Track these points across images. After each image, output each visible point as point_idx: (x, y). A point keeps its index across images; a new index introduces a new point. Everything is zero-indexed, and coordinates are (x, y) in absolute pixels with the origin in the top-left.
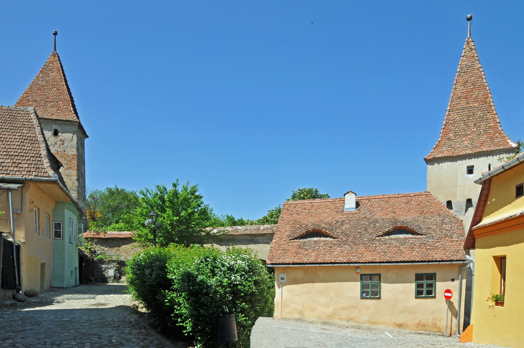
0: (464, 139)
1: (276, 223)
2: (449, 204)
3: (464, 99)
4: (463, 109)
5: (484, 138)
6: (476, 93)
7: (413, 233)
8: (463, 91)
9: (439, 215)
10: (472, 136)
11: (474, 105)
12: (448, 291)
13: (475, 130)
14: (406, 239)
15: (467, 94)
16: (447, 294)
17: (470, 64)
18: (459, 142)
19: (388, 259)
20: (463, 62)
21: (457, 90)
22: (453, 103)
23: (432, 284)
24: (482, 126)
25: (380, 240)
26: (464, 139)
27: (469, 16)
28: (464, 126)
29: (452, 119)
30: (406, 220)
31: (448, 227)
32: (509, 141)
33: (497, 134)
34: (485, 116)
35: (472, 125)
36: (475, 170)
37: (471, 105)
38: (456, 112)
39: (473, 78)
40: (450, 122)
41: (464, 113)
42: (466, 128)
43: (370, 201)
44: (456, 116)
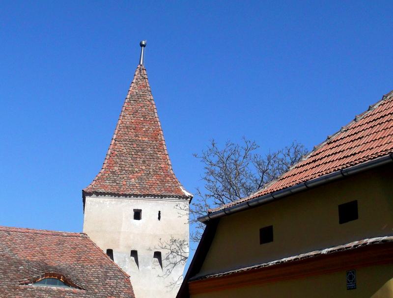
0: (131, 176)
1: (355, 288)
2: (110, 252)
3: (133, 131)
4: (132, 142)
5: (153, 179)
6: (147, 127)
7: (67, 283)
8: (133, 121)
9: (101, 266)
10: (140, 174)
14: (60, 292)
17: (141, 93)
20: (134, 89)
21: (126, 118)
25: (25, 289)
26: (131, 176)
28: (132, 161)
29: (118, 150)
30: (60, 266)
31: (113, 282)
32: (181, 188)
36: (143, 215)
37: (140, 139)
38: (124, 143)
39: (144, 110)
40: (116, 153)
43: (9, 234)
44: (122, 148)
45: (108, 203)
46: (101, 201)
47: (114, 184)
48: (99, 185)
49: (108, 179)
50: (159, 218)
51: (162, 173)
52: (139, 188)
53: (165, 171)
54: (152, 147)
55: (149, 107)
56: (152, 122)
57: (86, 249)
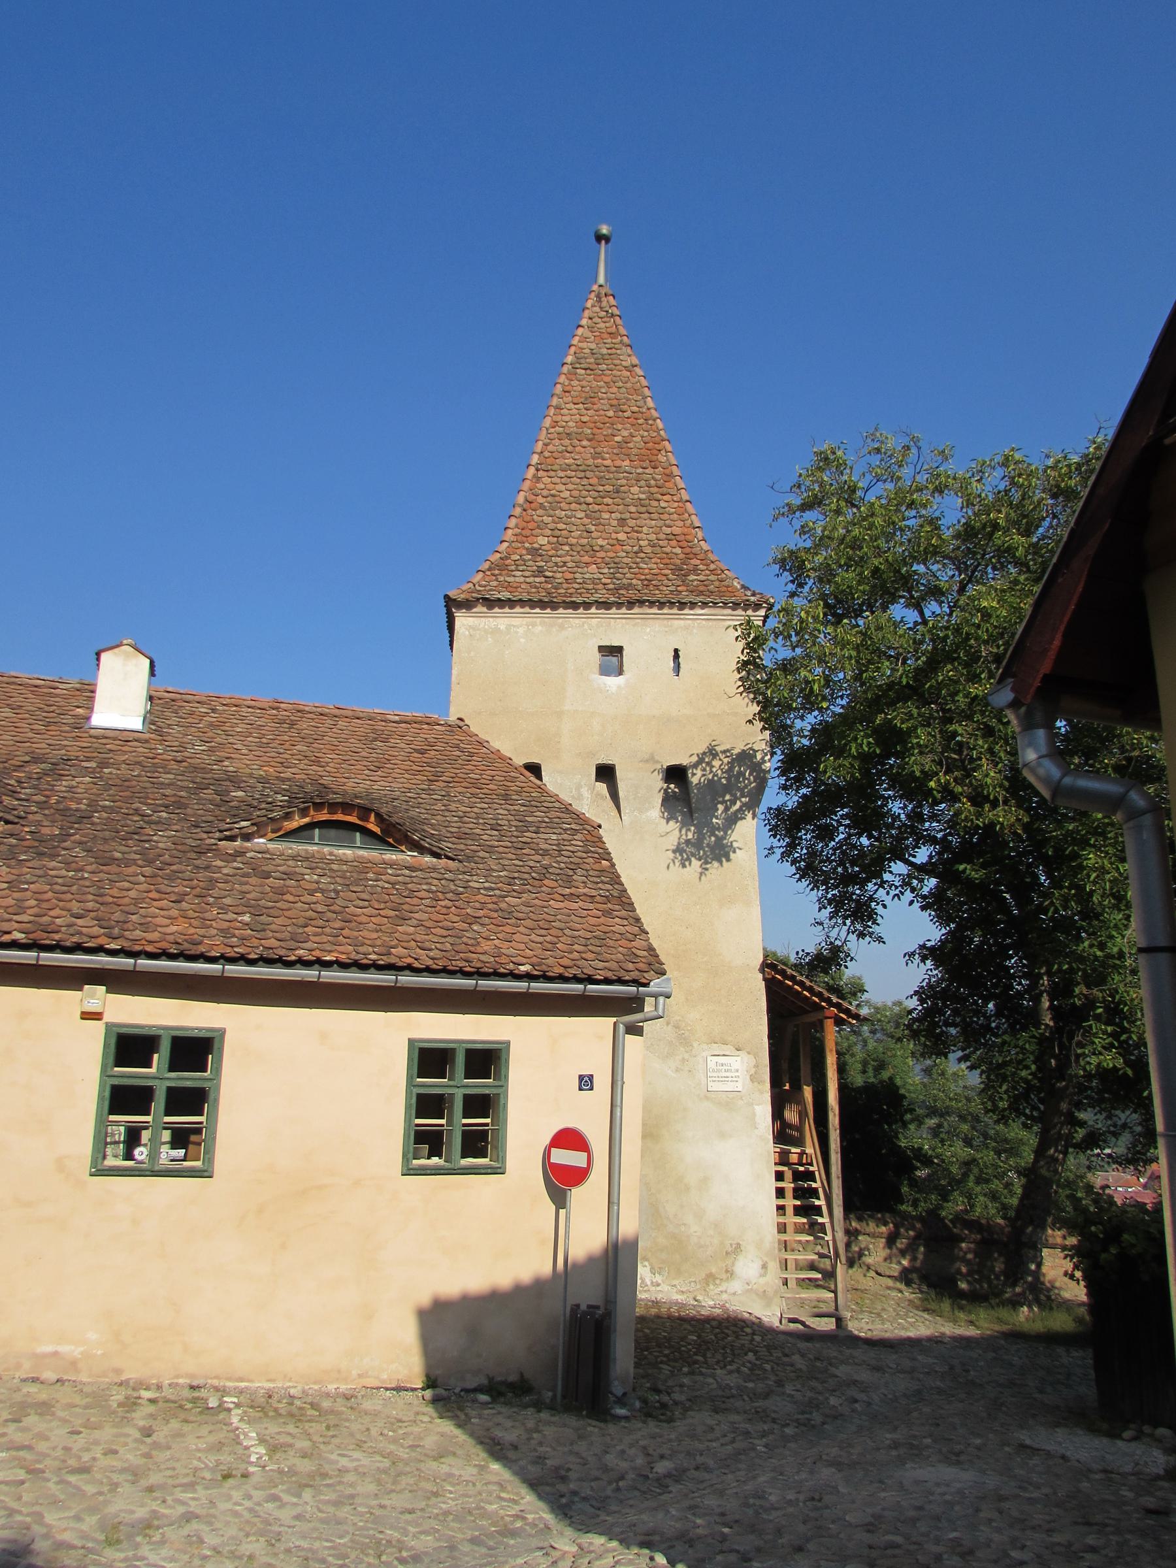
3: (585, 443)
8: (585, 419)
9: (506, 797)
11: (618, 463)
12: (568, 1138)
13: (622, 536)
14: (363, 867)
15: (596, 431)
16: (561, 1156)
17: (605, 351)
18: (569, 565)
19: (272, 943)
20: (583, 340)
21: (565, 411)
22: (550, 448)
23: (441, 1097)
24: (645, 530)
26: (586, 559)
27: (605, 230)
28: (586, 521)
29: (545, 493)
33: (695, 562)
34: (655, 503)
35: (615, 523)
38: (561, 474)
40: (540, 500)
41: (585, 482)
42: (593, 528)
45: (521, 630)
46: (502, 627)
47: (537, 580)
48: (495, 583)
49: (521, 568)
50: (677, 669)
51: (678, 550)
52: (611, 586)
53: (684, 544)
54: (642, 483)
55: (629, 385)
56: (640, 421)
57: (458, 753)
